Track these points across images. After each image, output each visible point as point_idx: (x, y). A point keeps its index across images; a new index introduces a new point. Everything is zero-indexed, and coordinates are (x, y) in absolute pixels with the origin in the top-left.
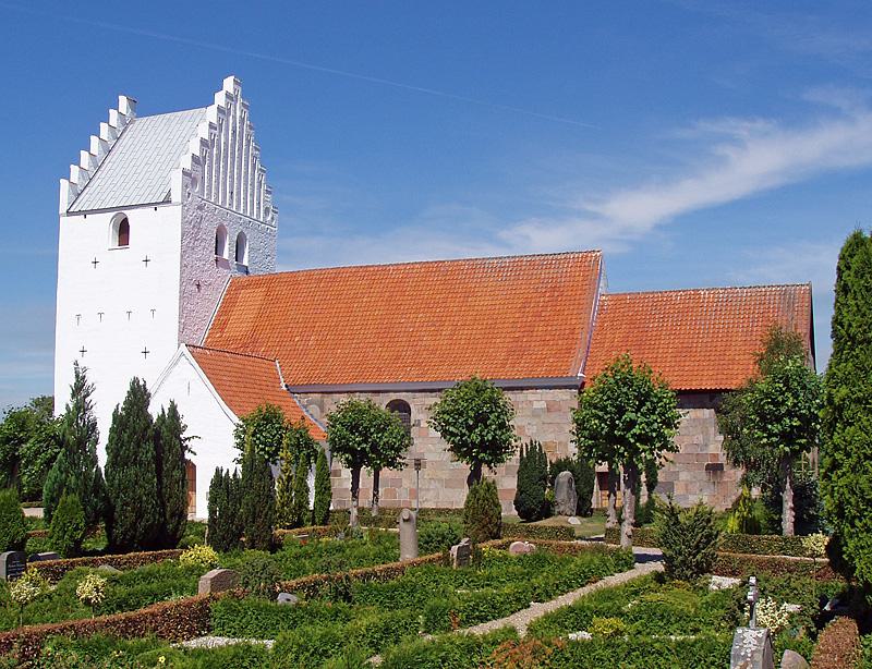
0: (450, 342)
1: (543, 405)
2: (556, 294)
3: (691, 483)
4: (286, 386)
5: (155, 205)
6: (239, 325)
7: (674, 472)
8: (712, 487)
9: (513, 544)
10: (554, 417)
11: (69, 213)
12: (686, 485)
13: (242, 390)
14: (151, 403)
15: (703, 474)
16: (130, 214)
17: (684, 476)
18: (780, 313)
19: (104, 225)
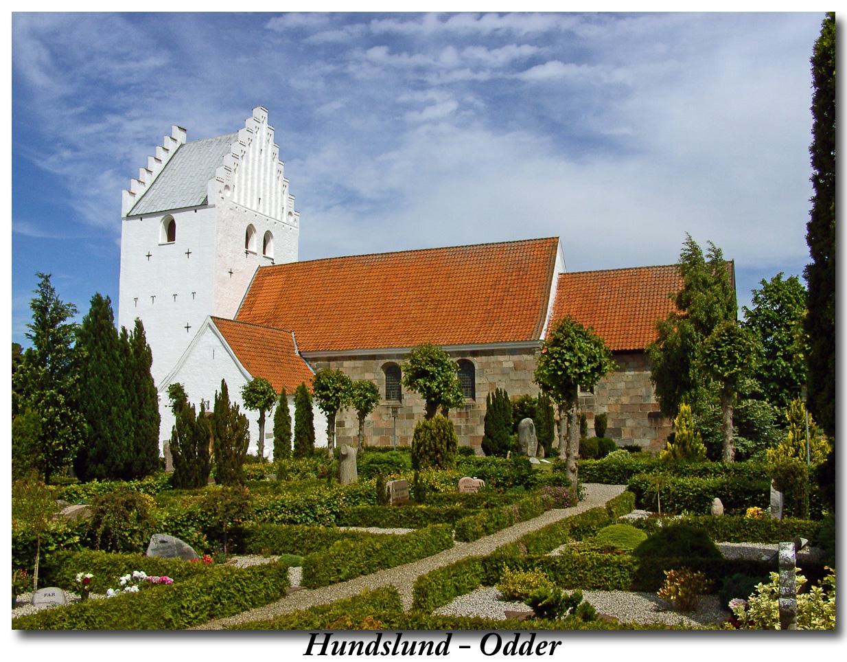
0: (433, 314)
1: (511, 365)
2: (521, 273)
3: (636, 428)
4: (299, 352)
5: (195, 208)
6: (262, 308)
7: (622, 420)
8: (654, 432)
9: (464, 478)
10: (521, 375)
11: (129, 217)
12: (632, 431)
13: (259, 354)
14: (808, 157)
15: (646, 422)
16: (176, 216)
17: (629, 423)
18: (643, 331)
19: (157, 227)
